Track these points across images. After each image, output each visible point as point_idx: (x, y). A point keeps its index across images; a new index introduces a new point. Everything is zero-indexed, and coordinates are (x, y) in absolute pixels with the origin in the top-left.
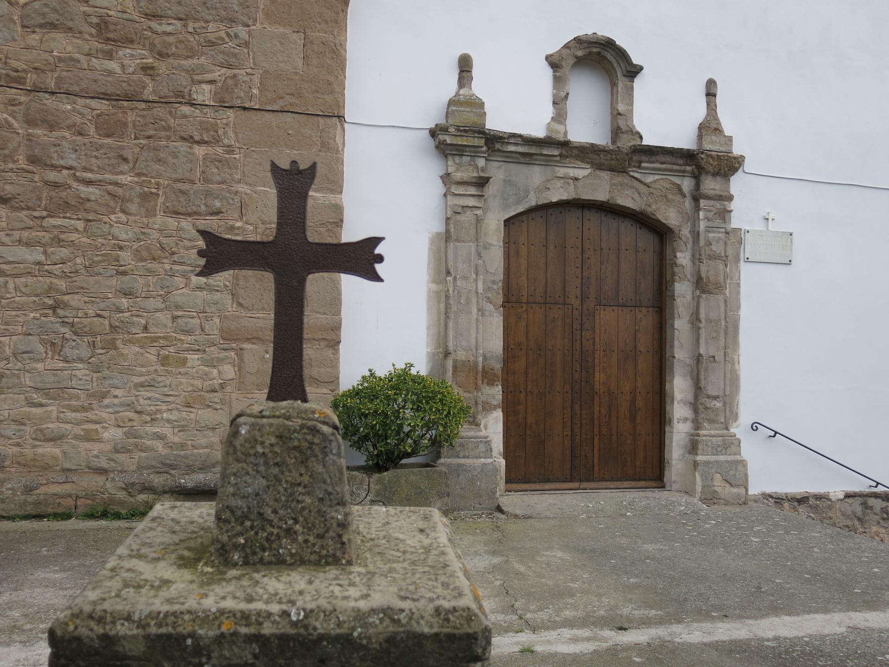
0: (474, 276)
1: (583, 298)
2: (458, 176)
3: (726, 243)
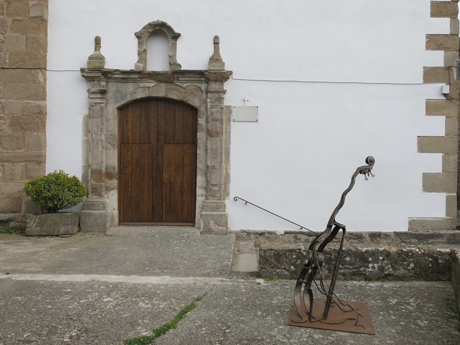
0: (100, 133)
1: (158, 141)
2: (93, 90)
3: (221, 113)
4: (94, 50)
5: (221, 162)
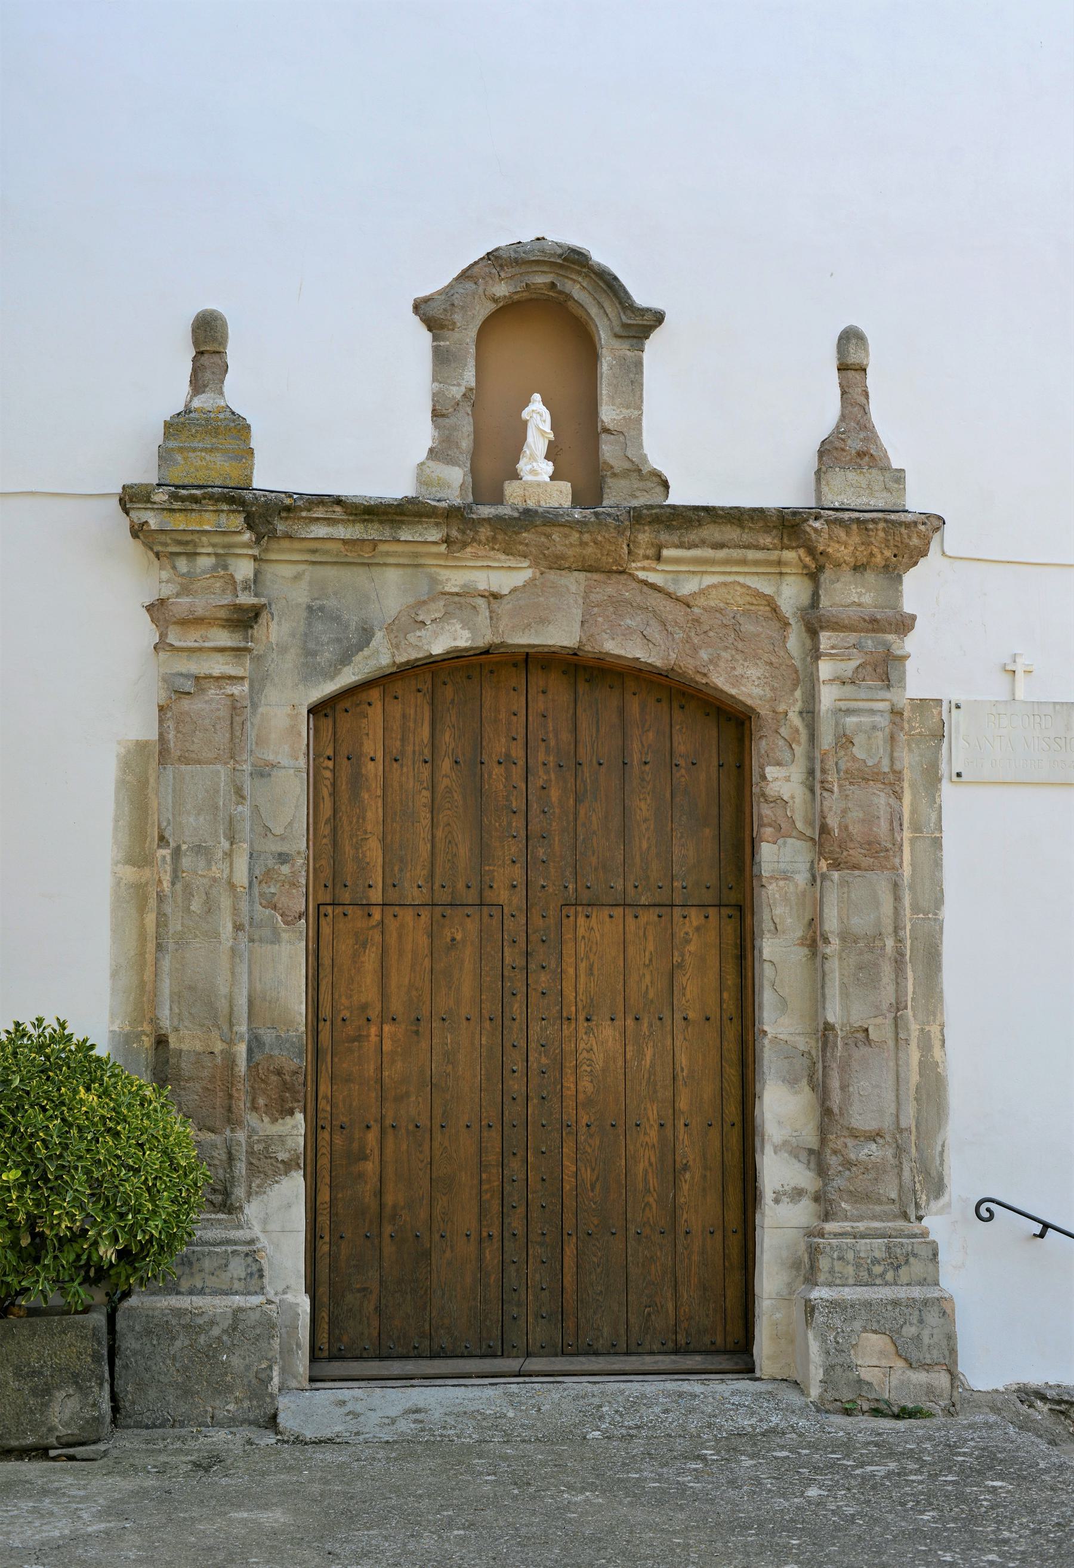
0: (226, 845)
4: (185, 388)
5: (898, 1006)
